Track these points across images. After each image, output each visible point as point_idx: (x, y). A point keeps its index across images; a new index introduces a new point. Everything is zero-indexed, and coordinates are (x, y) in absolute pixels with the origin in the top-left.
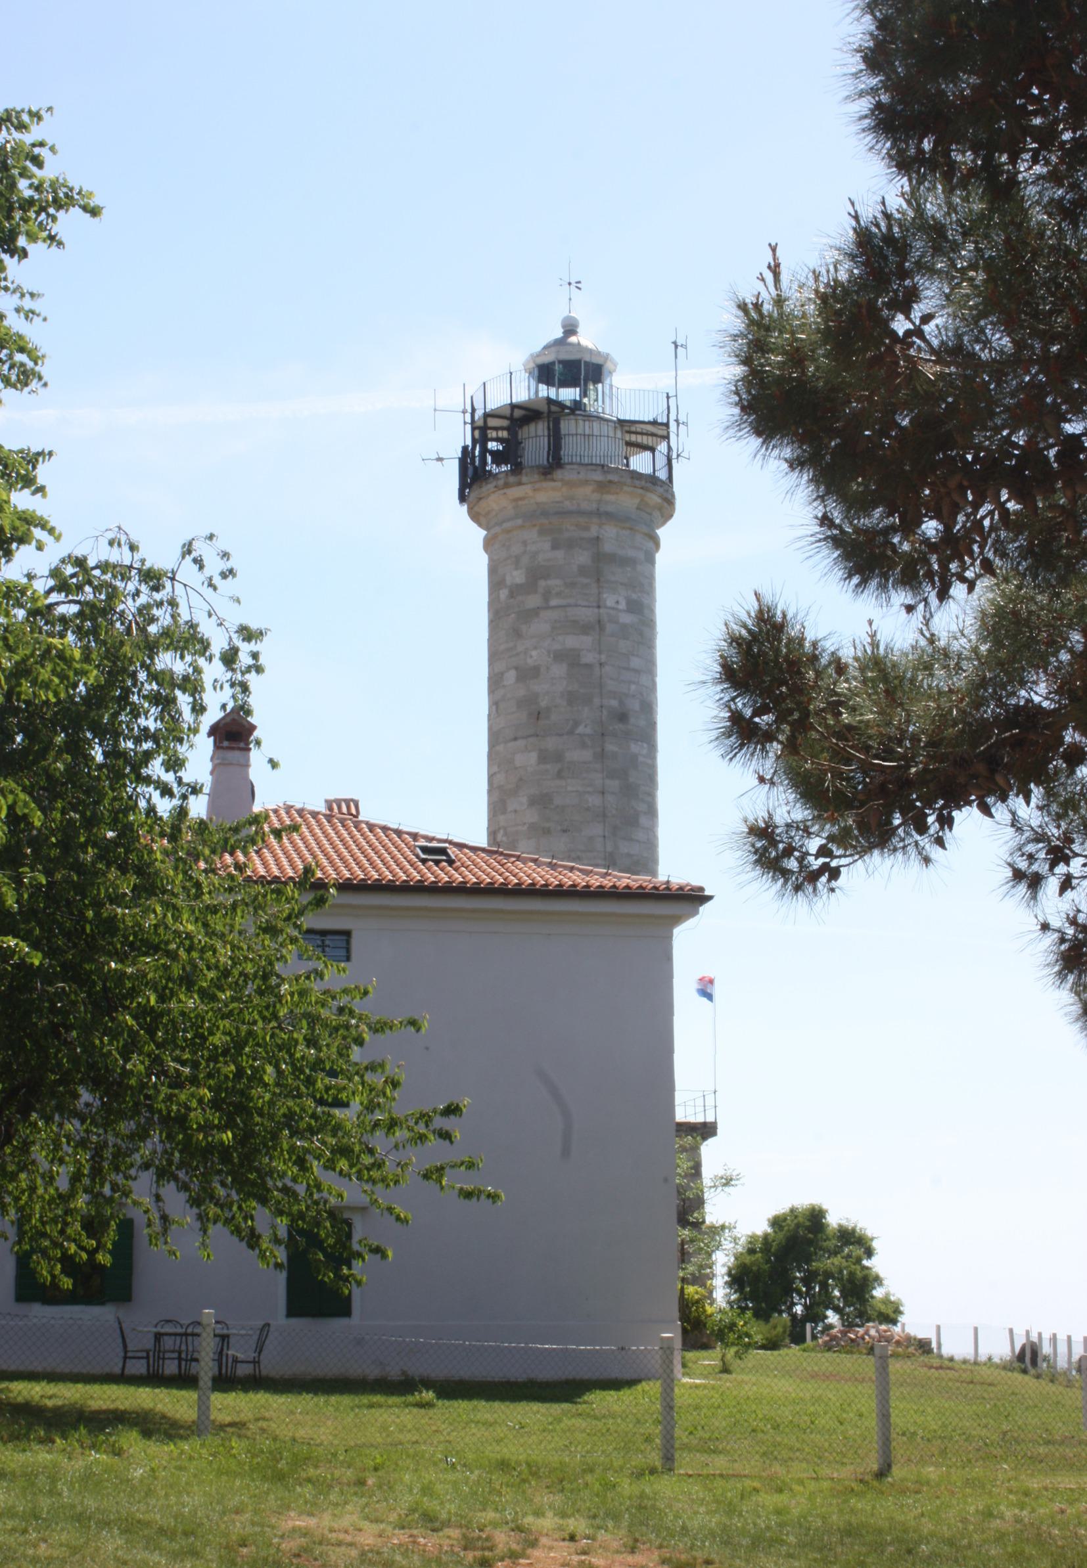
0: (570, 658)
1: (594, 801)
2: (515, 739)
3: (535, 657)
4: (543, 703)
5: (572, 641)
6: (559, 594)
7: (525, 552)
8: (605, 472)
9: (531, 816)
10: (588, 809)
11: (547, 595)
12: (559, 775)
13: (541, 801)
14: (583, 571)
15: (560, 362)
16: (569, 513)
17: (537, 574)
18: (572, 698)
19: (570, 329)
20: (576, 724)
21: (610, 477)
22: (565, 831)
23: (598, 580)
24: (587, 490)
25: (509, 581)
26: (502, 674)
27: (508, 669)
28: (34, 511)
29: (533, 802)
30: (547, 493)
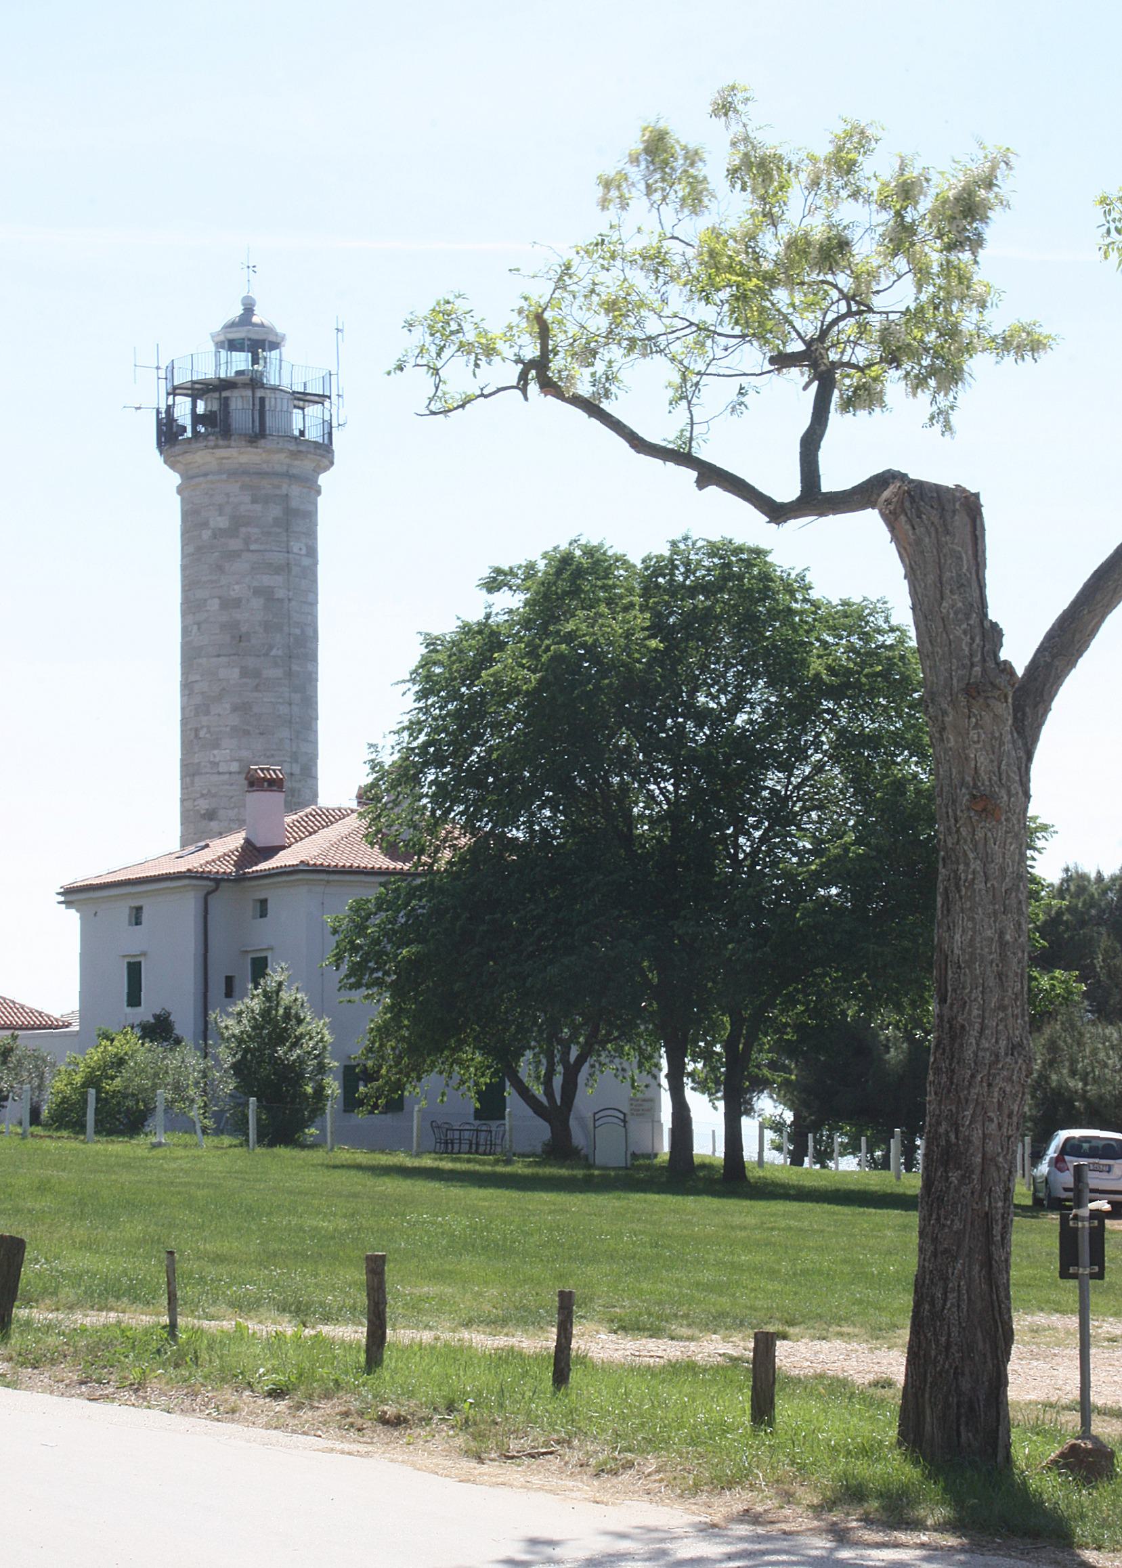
0: (266, 594)
1: (284, 710)
2: (219, 656)
3: (237, 591)
4: (244, 629)
5: (266, 580)
6: (256, 541)
7: (228, 502)
8: (298, 444)
9: (234, 720)
10: (279, 716)
11: (247, 541)
12: (256, 688)
13: (242, 708)
14: (277, 523)
15: (249, 339)
16: (267, 474)
17: (238, 522)
18: (267, 626)
19: (249, 310)
20: (271, 648)
21: (302, 448)
22: (261, 734)
23: (287, 530)
24: (282, 457)
25: (212, 524)
26: (206, 600)
27: (212, 597)
28: (431, 643)
29: (235, 709)
30: (239, 455)
